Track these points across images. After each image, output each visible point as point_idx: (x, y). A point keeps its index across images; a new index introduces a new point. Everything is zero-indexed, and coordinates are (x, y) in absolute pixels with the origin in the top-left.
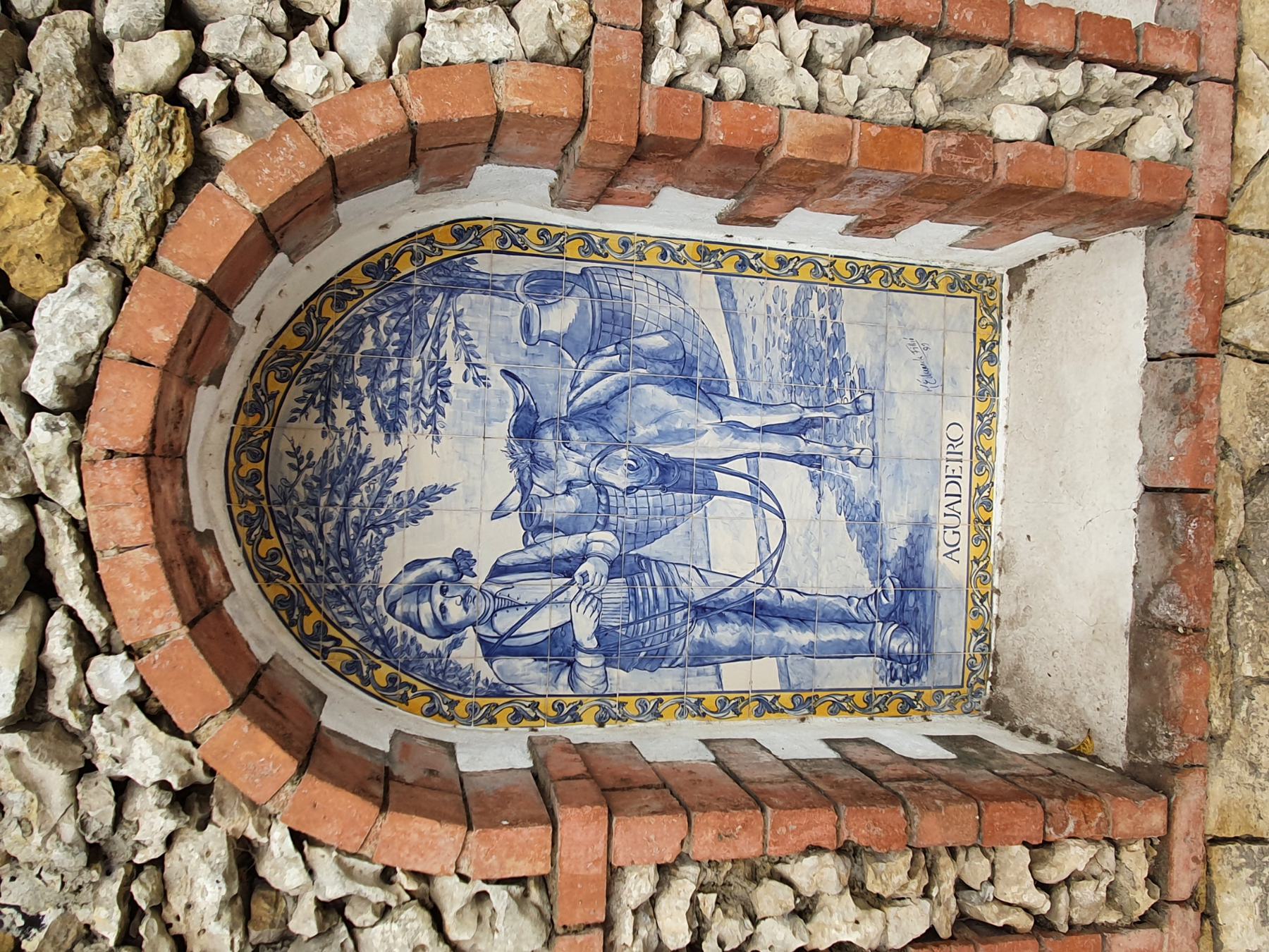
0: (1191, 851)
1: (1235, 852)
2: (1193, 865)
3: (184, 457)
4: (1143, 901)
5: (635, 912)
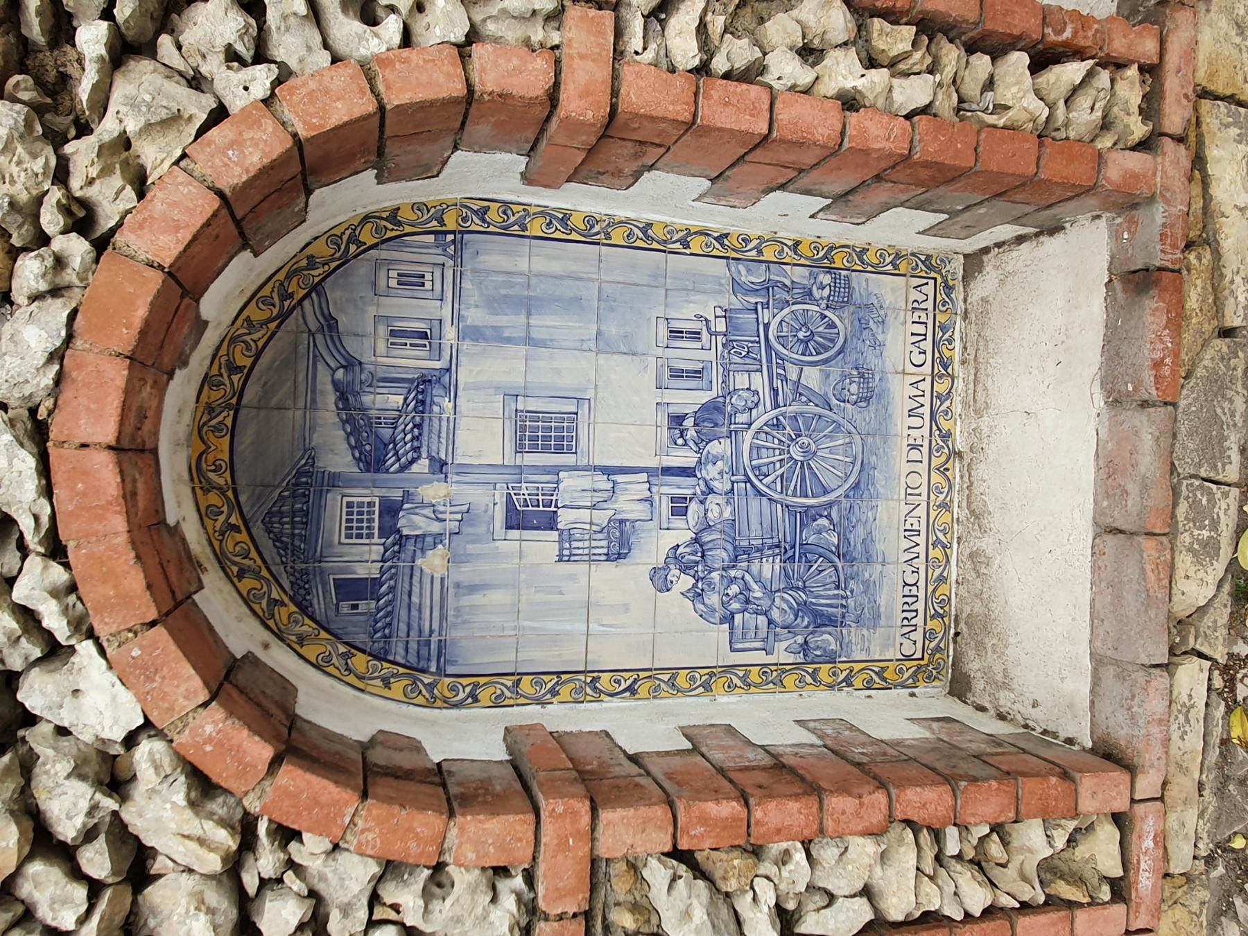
0: (1182, 87)
1: (1223, 109)
2: (1184, 102)
3: (155, 452)
4: (1139, 130)
5: (646, 17)
